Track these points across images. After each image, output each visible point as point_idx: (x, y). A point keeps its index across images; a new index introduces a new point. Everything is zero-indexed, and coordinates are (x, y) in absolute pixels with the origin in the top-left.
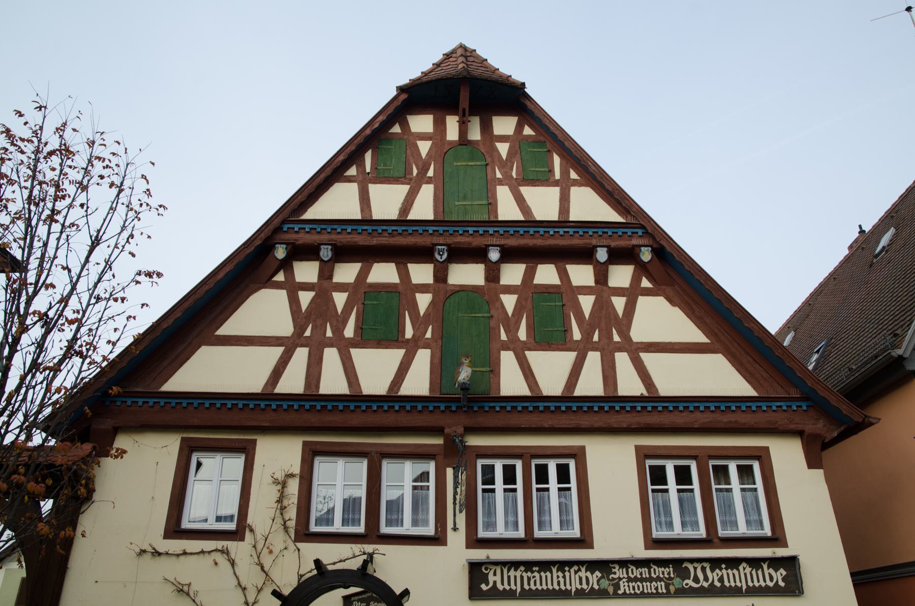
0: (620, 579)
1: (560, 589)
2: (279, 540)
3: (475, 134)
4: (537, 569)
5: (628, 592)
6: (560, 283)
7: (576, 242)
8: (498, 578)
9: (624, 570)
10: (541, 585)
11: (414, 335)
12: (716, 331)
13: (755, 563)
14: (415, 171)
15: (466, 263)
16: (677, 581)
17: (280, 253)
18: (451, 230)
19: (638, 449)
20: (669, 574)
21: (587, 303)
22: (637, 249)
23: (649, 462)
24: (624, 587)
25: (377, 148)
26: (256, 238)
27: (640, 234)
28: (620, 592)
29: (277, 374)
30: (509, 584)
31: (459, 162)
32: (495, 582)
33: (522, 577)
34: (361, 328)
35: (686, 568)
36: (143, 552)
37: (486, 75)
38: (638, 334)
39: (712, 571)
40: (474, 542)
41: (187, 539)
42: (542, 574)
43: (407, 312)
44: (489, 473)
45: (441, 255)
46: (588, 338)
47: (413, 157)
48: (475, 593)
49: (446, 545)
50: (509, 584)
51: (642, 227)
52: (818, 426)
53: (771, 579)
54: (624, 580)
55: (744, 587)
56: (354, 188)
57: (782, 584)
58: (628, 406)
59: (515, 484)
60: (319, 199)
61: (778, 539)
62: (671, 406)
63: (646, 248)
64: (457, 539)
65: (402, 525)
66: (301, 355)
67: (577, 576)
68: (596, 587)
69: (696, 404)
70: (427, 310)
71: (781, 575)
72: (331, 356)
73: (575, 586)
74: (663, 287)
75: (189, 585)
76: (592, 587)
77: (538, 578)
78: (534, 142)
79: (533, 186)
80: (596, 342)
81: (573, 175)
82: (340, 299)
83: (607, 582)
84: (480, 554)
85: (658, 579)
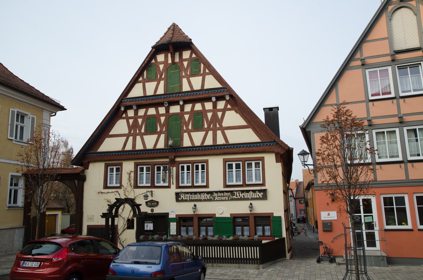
0: (215, 196)
1: (199, 199)
2: (129, 188)
3: (177, 60)
4: (193, 194)
5: (217, 200)
8: (183, 197)
9: (217, 194)
10: (194, 198)
11: (160, 130)
13: (254, 191)
14: (159, 76)
15: (175, 105)
16: (231, 197)
17: (123, 109)
18: (169, 96)
20: (229, 195)
21: (210, 115)
23: (227, 163)
24: (216, 198)
25: (148, 69)
26: (115, 106)
28: (215, 200)
29: (156, 91)
30: (186, 198)
31: (172, 71)
32: (182, 198)
33: (189, 196)
34: (146, 129)
36: (99, 192)
38: (225, 124)
39: (241, 193)
40: (178, 187)
41: (109, 189)
42: (195, 195)
43: (158, 123)
44: (183, 168)
45: (166, 105)
46: (209, 127)
47: (158, 71)
48: (177, 200)
49: (171, 188)
50: (186, 198)
52: (279, 150)
53: (258, 195)
54: (217, 196)
55: (250, 198)
56: (141, 84)
57: (261, 197)
58: (219, 147)
60: (132, 90)
61: (263, 184)
62: (232, 146)
63: (227, 96)
64: (173, 186)
65: (113, 184)
66: (131, 138)
67: (204, 195)
68: (209, 198)
69: (240, 146)
70: (164, 122)
71: (261, 194)
73: (203, 198)
74: (235, 107)
75: (110, 200)
76: (208, 199)
78: (195, 60)
79: (194, 77)
80: (211, 128)
81: (207, 71)
82: (140, 121)
83: (212, 197)
84: (179, 190)
85: (226, 196)
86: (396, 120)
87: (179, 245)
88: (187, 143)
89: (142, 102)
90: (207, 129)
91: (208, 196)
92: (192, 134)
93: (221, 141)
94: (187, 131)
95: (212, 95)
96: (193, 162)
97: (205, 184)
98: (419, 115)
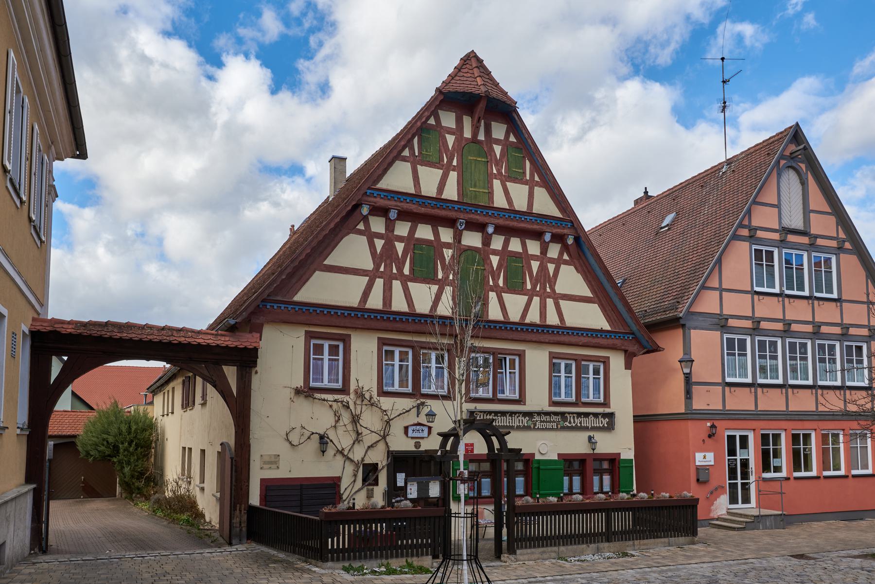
0: (537, 421)
3: (481, 137)
6: (522, 251)
7: (535, 227)
12: (597, 290)
13: (596, 415)
14: (445, 160)
19: (550, 353)
20: (558, 419)
21: (535, 265)
22: (566, 237)
24: (538, 425)
27: (569, 226)
28: (536, 427)
35: (566, 416)
37: (501, 97)
38: (559, 289)
39: (577, 418)
42: (502, 417)
45: (461, 226)
47: (444, 147)
51: (572, 222)
54: (539, 422)
57: (606, 425)
58: (551, 330)
59: (338, 356)
60: (388, 172)
61: (606, 404)
63: (572, 236)
66: (379, 283)
68: (526, 425)
72: (397, 285)
73: (516, 424)
77: (500, 420)
80: (538, 291)
81: (537, 178)
82: (400, 247)
83: (531, 422)
85: (554, 422)
86: (809, 328)
87: (628, 499)
88: (494, 313)
89: (412, 208)
90: (530, 293)
91: (525, 421)
92: (505, 296)
93: (552, 319)
94: (495, 290)
95: (545, 228)
96: (577, 359)
97: (516, 396)
98: (802, 324)
